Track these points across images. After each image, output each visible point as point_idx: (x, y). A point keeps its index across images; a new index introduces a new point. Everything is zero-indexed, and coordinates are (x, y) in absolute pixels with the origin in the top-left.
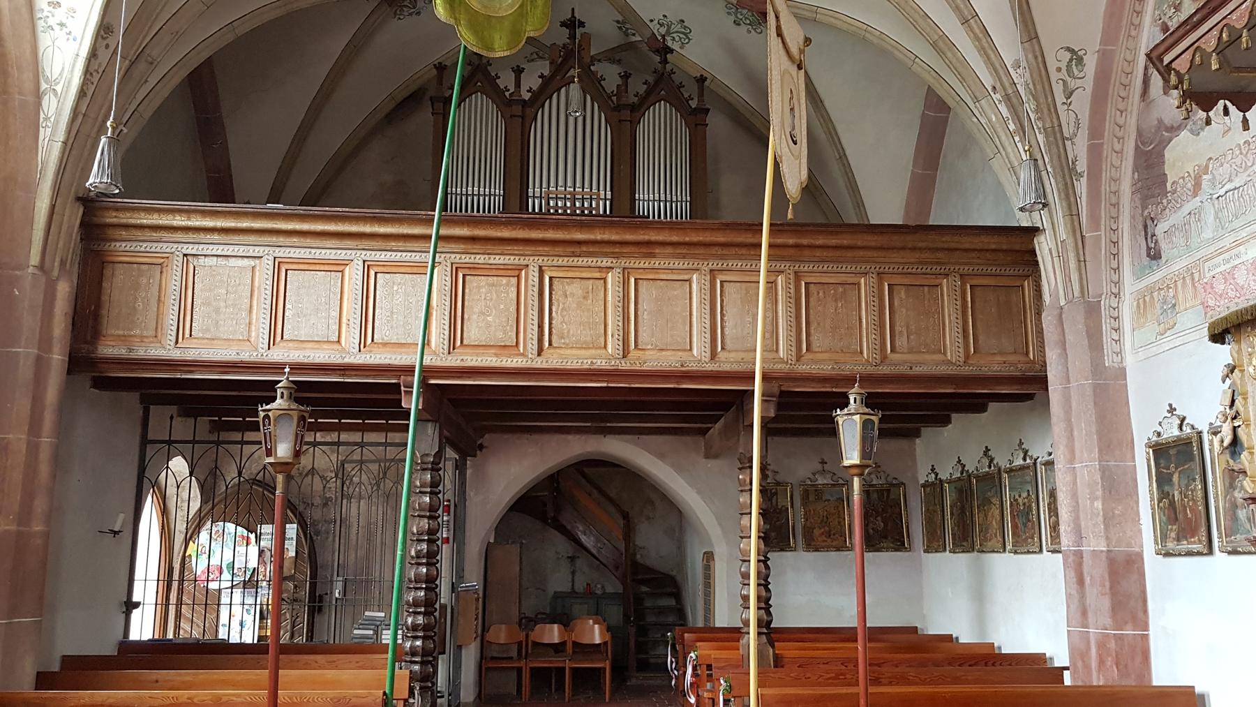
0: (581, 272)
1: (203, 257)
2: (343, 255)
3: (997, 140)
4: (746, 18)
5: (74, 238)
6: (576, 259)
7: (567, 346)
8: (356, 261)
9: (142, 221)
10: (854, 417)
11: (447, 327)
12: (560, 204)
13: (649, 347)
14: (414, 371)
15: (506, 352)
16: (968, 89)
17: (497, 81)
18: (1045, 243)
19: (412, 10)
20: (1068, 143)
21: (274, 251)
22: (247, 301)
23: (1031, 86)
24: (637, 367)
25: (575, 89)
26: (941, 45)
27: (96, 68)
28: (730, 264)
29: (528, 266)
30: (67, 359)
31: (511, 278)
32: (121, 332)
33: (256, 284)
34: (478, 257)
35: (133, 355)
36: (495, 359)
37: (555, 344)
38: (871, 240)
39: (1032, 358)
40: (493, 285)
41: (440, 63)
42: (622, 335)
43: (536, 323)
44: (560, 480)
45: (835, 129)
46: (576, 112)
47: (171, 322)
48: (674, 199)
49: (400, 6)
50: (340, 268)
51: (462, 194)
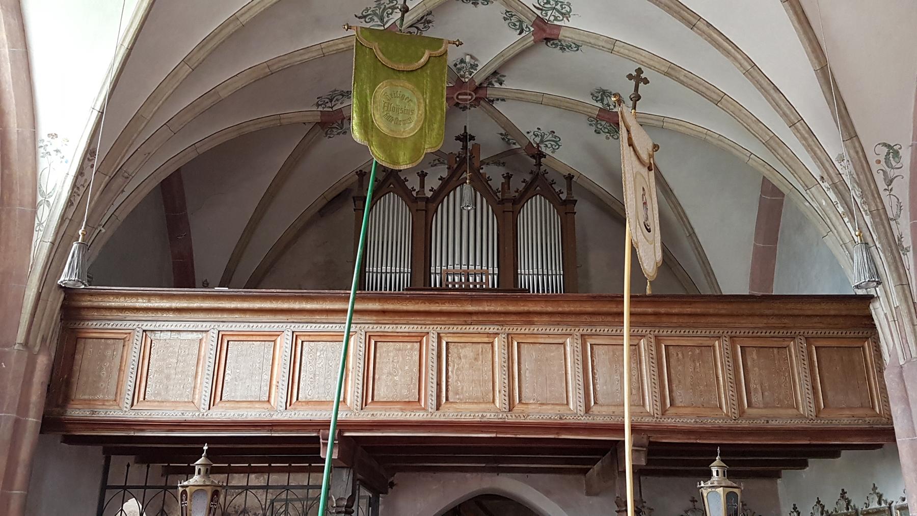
0: (473, 337)
1: (159, 332)
2: (275, 327)
3: (829, 221)
4: (605, 128)
5: (55, 318)
6: (468, 327)
7: (462, 402)
8: (286, 332)
9: (110, 304)
10: (718, 490)
11: (360, 387)
12: (457, 279)
13: (532, 401)
14: (330, 425)
15: (409, 407)
16: (799, 179)
17: (406, 183)
18: (880, 309)
19: (339, 131)
20: (892, 223)
21: (219, 326)
22: (194, 368)
23: (855, 176)
24: (522, 420)
25: (467, 189)
26: (773, 144)
27: (82, 183)
28: (598, 330)
29: (428, 333)
30: (40, 421)
31: (415, 344)
32: (86, 397)
33: (202, 353)
34: (387, 326)
35: (96, 417)
36: (400, 414)
37: (451, 400)
38: (723, 308)
39: (878, 412)
40: (399, 350)
41: (361, 171)
42: (507, 391)
43: (435, 381)
44: (461, 511)
45: (684, 213)
46: (468, 206)
47: (129, 388)
48: (550, 273)
49: (330, 128)
50: (273, 338)
51: (377, 272)
